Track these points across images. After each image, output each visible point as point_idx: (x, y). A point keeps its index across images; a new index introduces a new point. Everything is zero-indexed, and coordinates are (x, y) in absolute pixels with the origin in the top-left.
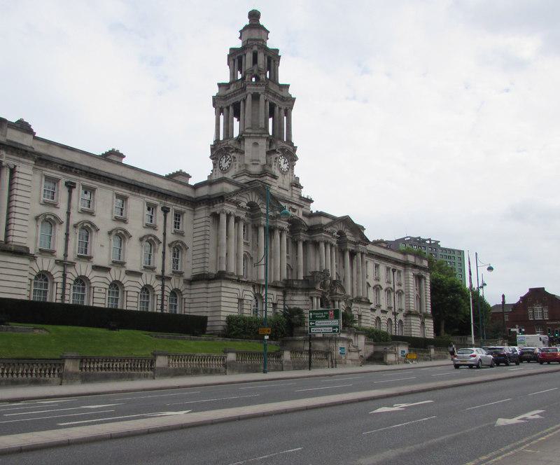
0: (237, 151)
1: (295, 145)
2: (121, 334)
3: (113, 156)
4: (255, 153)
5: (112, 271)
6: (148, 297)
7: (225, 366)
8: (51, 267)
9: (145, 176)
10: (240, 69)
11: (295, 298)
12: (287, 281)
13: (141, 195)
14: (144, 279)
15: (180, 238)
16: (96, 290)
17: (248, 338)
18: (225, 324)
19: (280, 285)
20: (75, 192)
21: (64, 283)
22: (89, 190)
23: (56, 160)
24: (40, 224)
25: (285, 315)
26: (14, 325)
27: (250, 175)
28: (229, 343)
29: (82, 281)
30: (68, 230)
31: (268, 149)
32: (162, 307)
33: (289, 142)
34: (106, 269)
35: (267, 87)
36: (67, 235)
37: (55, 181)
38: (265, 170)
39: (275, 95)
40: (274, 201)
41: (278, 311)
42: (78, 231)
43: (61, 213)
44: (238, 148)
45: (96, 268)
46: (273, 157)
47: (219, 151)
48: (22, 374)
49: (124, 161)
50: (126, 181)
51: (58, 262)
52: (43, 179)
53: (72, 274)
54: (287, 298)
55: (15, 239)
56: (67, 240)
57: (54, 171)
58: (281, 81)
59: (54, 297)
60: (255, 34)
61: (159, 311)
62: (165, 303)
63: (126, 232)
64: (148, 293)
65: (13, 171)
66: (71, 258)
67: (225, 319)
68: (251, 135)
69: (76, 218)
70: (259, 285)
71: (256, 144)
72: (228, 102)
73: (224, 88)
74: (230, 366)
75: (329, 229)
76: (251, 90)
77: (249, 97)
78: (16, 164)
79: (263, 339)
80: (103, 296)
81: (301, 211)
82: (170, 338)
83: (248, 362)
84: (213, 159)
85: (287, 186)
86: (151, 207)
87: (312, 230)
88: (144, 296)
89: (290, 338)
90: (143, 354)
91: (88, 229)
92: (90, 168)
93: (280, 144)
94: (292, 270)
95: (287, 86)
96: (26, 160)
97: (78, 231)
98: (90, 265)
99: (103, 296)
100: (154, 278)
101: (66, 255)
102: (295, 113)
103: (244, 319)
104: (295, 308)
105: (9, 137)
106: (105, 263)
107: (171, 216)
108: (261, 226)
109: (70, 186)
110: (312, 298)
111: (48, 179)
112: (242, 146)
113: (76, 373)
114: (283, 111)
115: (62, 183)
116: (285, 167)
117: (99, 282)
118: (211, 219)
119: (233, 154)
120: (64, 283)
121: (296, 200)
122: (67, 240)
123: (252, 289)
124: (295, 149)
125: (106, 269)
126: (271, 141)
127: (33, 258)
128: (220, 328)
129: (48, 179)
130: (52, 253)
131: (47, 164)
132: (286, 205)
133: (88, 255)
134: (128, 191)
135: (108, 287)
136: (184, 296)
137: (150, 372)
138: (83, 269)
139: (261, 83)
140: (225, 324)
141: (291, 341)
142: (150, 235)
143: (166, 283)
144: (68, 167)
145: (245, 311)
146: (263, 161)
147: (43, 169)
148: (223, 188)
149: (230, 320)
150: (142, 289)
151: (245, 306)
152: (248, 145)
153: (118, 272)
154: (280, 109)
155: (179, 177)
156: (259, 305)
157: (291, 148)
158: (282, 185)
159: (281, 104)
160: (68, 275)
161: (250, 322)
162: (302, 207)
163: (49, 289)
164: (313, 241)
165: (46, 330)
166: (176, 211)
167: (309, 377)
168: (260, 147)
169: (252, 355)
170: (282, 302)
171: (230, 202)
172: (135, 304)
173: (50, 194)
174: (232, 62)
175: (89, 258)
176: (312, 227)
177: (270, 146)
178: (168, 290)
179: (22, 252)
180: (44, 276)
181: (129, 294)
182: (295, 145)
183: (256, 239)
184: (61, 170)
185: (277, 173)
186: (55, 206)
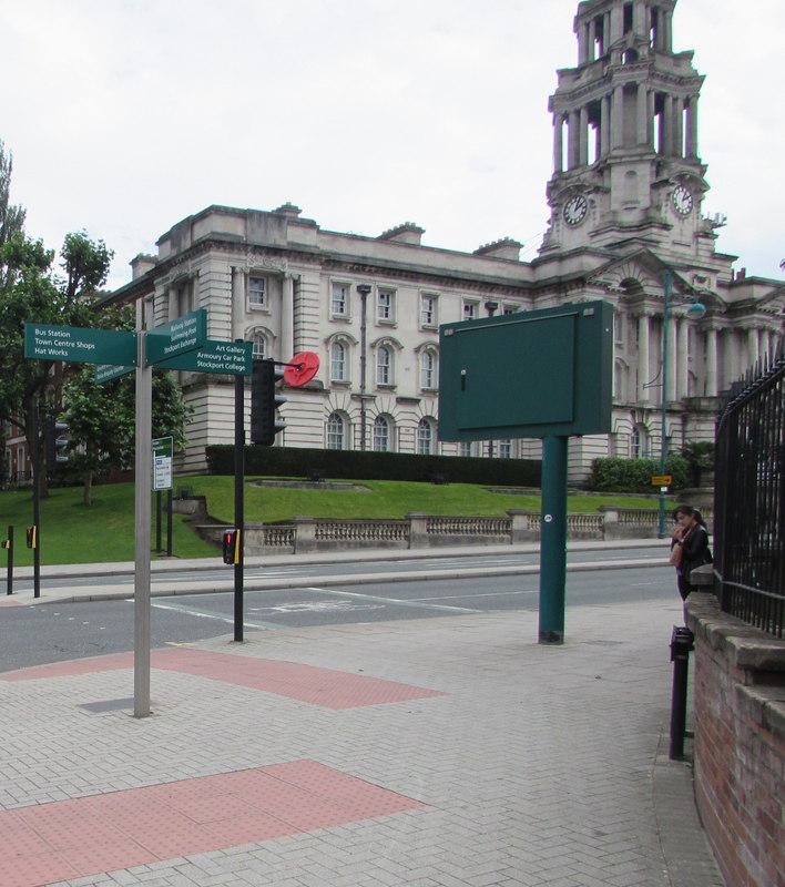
0: (597, 189)
1: (703, 163)
2: (453, 488)
3: (403, 235)
4: (630, 189)
5: (422, 403)
6: (341, 428)
7: (603, 528)
8: (346, 405)
9: (358, 244)
10: (599, 36)
11: (703, 427)
12: (689, 400)
13: (456, 290)
14: (423, 409)
16: (403, 430)
17: (626, 492)
18: (590, 471)
19: (676, 407)
20: (369, 298)
21: (363, 424)
22: (387, 295)
23: (344, 259)
24: (330, 347)
25: (685, 454)
26: (328, 481)
27: (623, 228)
28: (600, 499)
29: (384, 419)
30: (364, 352)
31: (654, 180)
32: (363, 443)
33: (693, 159)
34: (415, 402)
35: (652, 67)
36: (363, 359)
37: (345, 287)
38: (647, 218)
39: (666, 78)
40: (663, 271)
41: (673, 448)
42: (376, 352)
43: (354, 330)
44: (599, 184)
45: (402, 401)
46: (663, 191)
47: (563, 191)
48: (355, 536)
49: (425, 241)
50: (435, 272)
51: (355, 397)
52: (331, 287)
53: (373, 411)
54: (690, 427)
56: (363, 366)
57: (343, 274)
58: (677, 49)
59: (352, 443)
61: (358, 449)
62: (367, 436)
63: (395, 342)
64: (385, 424)
65: (296, 283)
66: (369, 390)
67: (589, 463)
68: (624, 160)
69: (373, 335)
70: (642, 410)
71: (631, 174)
72: (579, 102)
73: (570, 78)
74: (609, 528)
75: (767, 306)
76: (620, 79)
77: (619, 93)
79: (660, 493)
80: (411, 438)
81: (714, 279)
82: (515, 493)
83: (634, 524)
84: (553, 206)
85: (688, 238)
87: (733, 310)
88: (423, 432)
89: (695, 489)
90: (493, 513)
92: (387, 261)
93: (676, 167)
94: (695, 379)
95: (688, 55)
96: (312, 266)
97: (376, 352)
98: (393, 398)
99: (411, 438)
101: (363, 387)
103: (620, 463)
104: (703, 443)
105: (290, 239)
106: (412, 394)
108: (643, 315)
109: (364, 291)
111: (336, 285)
112: (606, 180)
113: (424, 536)
114: (680, 103)
115: (353, 289)
116: (683, 206)
119: (590, 196)
120: (363, 424)
121: (704, 261)
122: (363, 366)
123: (629, 417)
124: (703, 169)
125: (415, 402)
126: (659, 166)
127: (326, 393)
128: (583, 477)
129: (336, 285)
130: (346, 385)
131: (453, 284)
132: (686, 277)
133: (389, 383)
134: (437, 287)
135: (417, 425)
136: (651, 433)
137: (506, 536)
138: (385, 403)
139: (641, 65)
140: (590, 471)
141: (696, 494)
143: (370, 406)
144: (360, 266)
145: (620, 451)
146: (645, 202)
147: (331, 272)
148: (582, 264)
149: (597, 464)
150: (420, 423)
151: (620, 444)
152: (617, 177)
153: (429, 404)
154: (675, 100)
155: (500, 250)
156: (641, 441)
157: (697, 171)
158: (678, 239)
159: (675, 89)
160: (368, 413)
161: (630, 468)
162: (716, 272)
163: (344, 433)
164: (735, 329)
165: (365, 486)
166: (381, 289)
167: (660, 546)
168: (639, 178)
169: (639, 513)
170: (680, 435)
171: (595, 285)
172: (411, 445)
173: (259, 297)
174: (583, 28)
175: (392, 388)
176: (734, 304)
177: (658, 173)
179: (317, 390)
180: (338, 416)
182: (703, 163)
183: (634, 337)
184: (352, 270)
185: (671, 219)
186: (346, 321)
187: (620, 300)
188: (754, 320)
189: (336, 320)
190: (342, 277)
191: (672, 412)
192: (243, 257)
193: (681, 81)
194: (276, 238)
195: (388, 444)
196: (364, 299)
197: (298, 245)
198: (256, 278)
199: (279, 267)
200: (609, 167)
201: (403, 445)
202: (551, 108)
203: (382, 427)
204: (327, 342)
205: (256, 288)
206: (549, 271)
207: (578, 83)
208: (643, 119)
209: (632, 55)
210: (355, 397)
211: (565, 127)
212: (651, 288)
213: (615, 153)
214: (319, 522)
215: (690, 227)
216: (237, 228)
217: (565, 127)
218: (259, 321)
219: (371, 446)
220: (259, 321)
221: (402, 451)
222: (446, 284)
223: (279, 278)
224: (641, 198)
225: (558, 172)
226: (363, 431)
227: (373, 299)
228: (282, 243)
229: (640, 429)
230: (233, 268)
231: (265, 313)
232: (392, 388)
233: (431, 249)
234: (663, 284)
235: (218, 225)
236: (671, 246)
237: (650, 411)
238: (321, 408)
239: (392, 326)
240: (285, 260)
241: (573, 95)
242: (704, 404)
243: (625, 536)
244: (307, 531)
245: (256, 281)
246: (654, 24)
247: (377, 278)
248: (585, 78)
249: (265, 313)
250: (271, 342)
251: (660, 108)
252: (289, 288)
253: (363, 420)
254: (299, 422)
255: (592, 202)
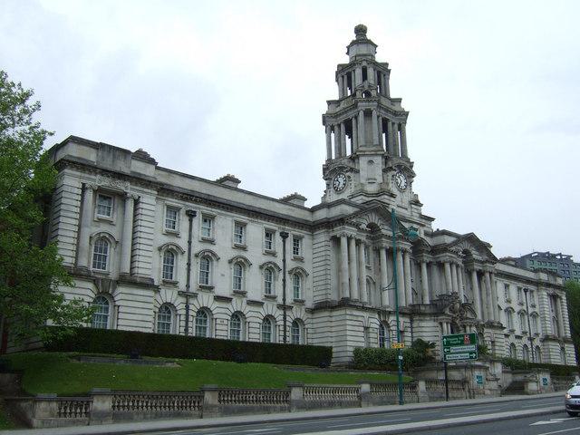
0: (352, 170)
3: (228, 182)
4: (370, 173)
9: (188, 181)
11: (423, 324)
12: (413, 306)
15: (299, 265)
16: (218, 321)
20: (195, 221)
21: (187, 315)
27: (367, 195)
29: (204, 312)
30: (189, 259)
31: (384, 167)
34: (228, 300)
35: (379, 102)
36: (189, 264)
39: (387, 110)
40: (391, 218)
43: (182, 243)
45: (218, 298)
46: (390, 174)
47: (331, 171)
49: (240, 186)
53: (195, 305)
54: (415, 325)
55: (140, 271)
56: (189, 270)
58: (393, 95)
59: (177, 328)
60: (363, 49)
62: (190, 324)
65: (137, 202)
66: (193, 288)
67: (352, 349)
69: (198, 247)
71: (371, 162)
72: (339, 120)
75: (453, 248)
76: (362, 106)
77: (361, 114)
78: (140, 194)
80: (225, 328)
84: (326, 180)
85: (406, 204)
86: (173, 211)
87: (435, 250)
91: (208, 258)
93: (396, 161)
95: (399, 100)
97: (199, 260)
99: (225, 328)
100: (275, 308)
101: (188, 286)
102: (409, 128)
105: (133, 169)
107: (290, 241)
109: (191, 215)
110: (441, 324)
113: (215, 406)
114: (396, 126)
115: (183, 212)
117: (221, 312)
118: (330, 243)
119: (348, 174)
121: (416, 218)
122: (189, 270)
123: (377, 316)
125: (228, 300)
126: (386, 159)
128: (348, 359)
129: (169, 208)
130: (175, 284)
135: (261, 321)
138: (205, 300)
142: (270, 263)
143: (191, 301)
144: (188, 196)
149: (357, 351)
150: (264, 320)
152: (363, 162)
153: (239, 302)
154: (393, 124)
155: (294, 200)
158: (400, 204)
159: (393, 119)
160: (191, 307)
162: (423, 226)
170: (409, 330)
171: (350, 224)
172: (257, 336)
174: (340, 79)
176: (436, 246)
178: (290, 320)
180: (167, 308)
181: (251, 325)
184: (182, 199)
185: (395, 191)
186: (176, 235)
187: (368, 237)
188: (444, 257)
189: (168, 234)
190: (174, 202)
191: (404, 314)
192: (93, 177)
193: (395, 114)
194: (121, 166)
195: (109, 321)
196: (191, 221)
197: (140, 174)
198: (103, 195)
199: (123, 188)
200: (358, 157)
201: (218, 332)
202: (324, 123)
203: (203, 318)
204: (160, 249)
205: (105, 203)
206: (321, 215)
207: (338, 109)
208: (376, 138)
209: (368, 94)
210: (181, 294)
211: (333, 135)
212: (386, 231)
213: (360, 149)
214: (114, 394)
215: (406, 198)
216: (92, 156)
217: (333, 135)
218: (104, 228)
219: (192, 332)
220: (104, 228)
221: (251, 340)
222: (253, 216)
223: (123, 197)
224: (377, 177)
225: (329, 160)
226: (285, 331)
227: (197, 221)
228: (126, 171)
229: (384, 325)
230: (84, 184)
231: (110, 223)
232: (211, 289)
233: (242, 191)
234: (393, 227)
235: (74, 151)
236: (397, 205)
237: (390, 312)
238: (152, 300)
239: (212, 242)
240: (128, 184)
241: (336, 115)
242: (422, 308)
243: (375, 404)
244: (104, 402)
245: (105, 198)
246: (379, 83)
247: (201, 207)
248: (343, 105)
249: (110, 223)
250: (113, 245)
251: (385, 129)
252: (130, 206)
253: (187, 313)
254: (133, 310)
255: (349, 177)
